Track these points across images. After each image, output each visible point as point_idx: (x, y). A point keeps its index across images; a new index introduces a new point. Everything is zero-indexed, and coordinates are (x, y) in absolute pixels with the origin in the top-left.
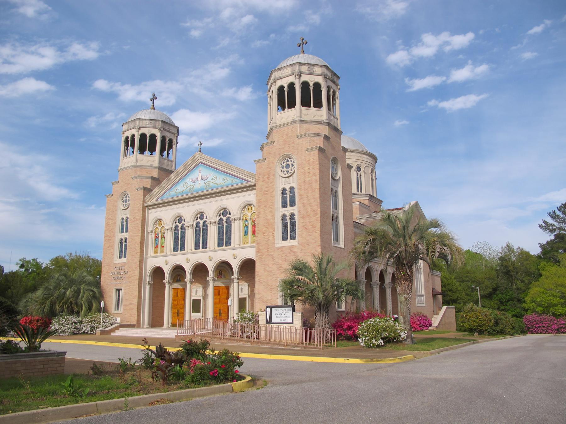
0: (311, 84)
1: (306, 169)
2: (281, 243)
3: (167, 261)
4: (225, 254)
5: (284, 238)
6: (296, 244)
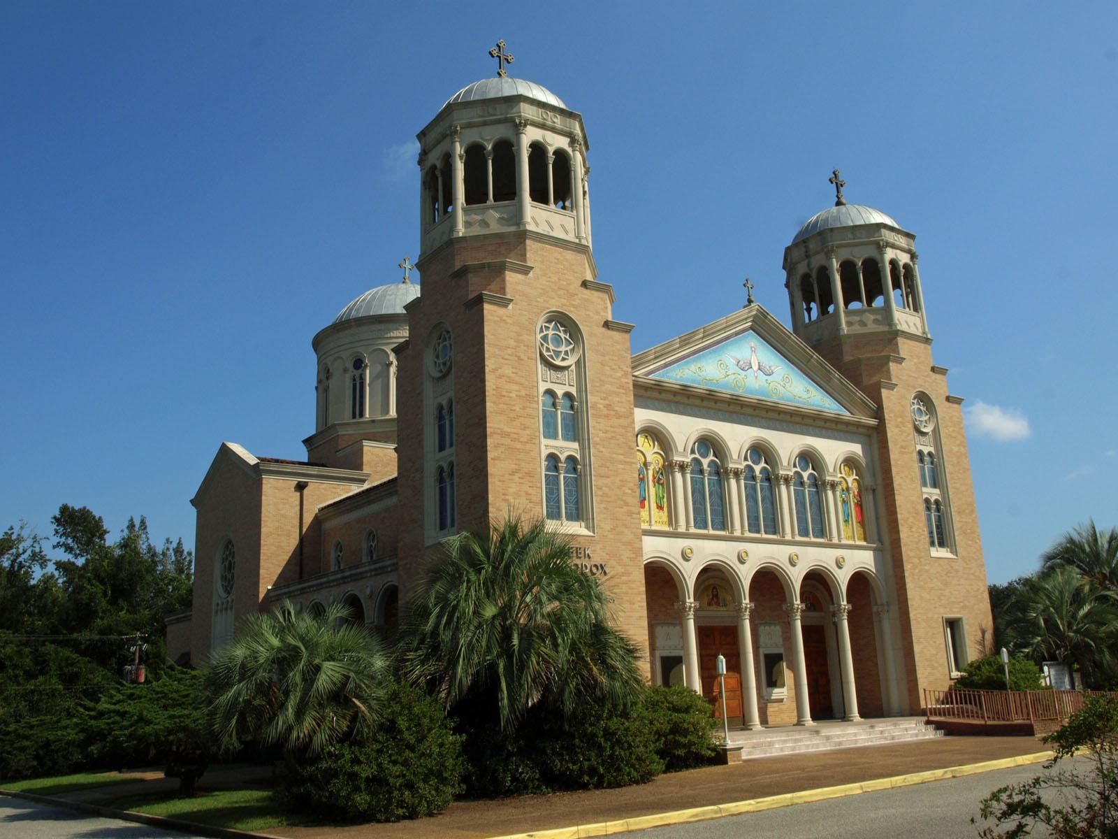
0: (551, 150)
1: (951, 429)
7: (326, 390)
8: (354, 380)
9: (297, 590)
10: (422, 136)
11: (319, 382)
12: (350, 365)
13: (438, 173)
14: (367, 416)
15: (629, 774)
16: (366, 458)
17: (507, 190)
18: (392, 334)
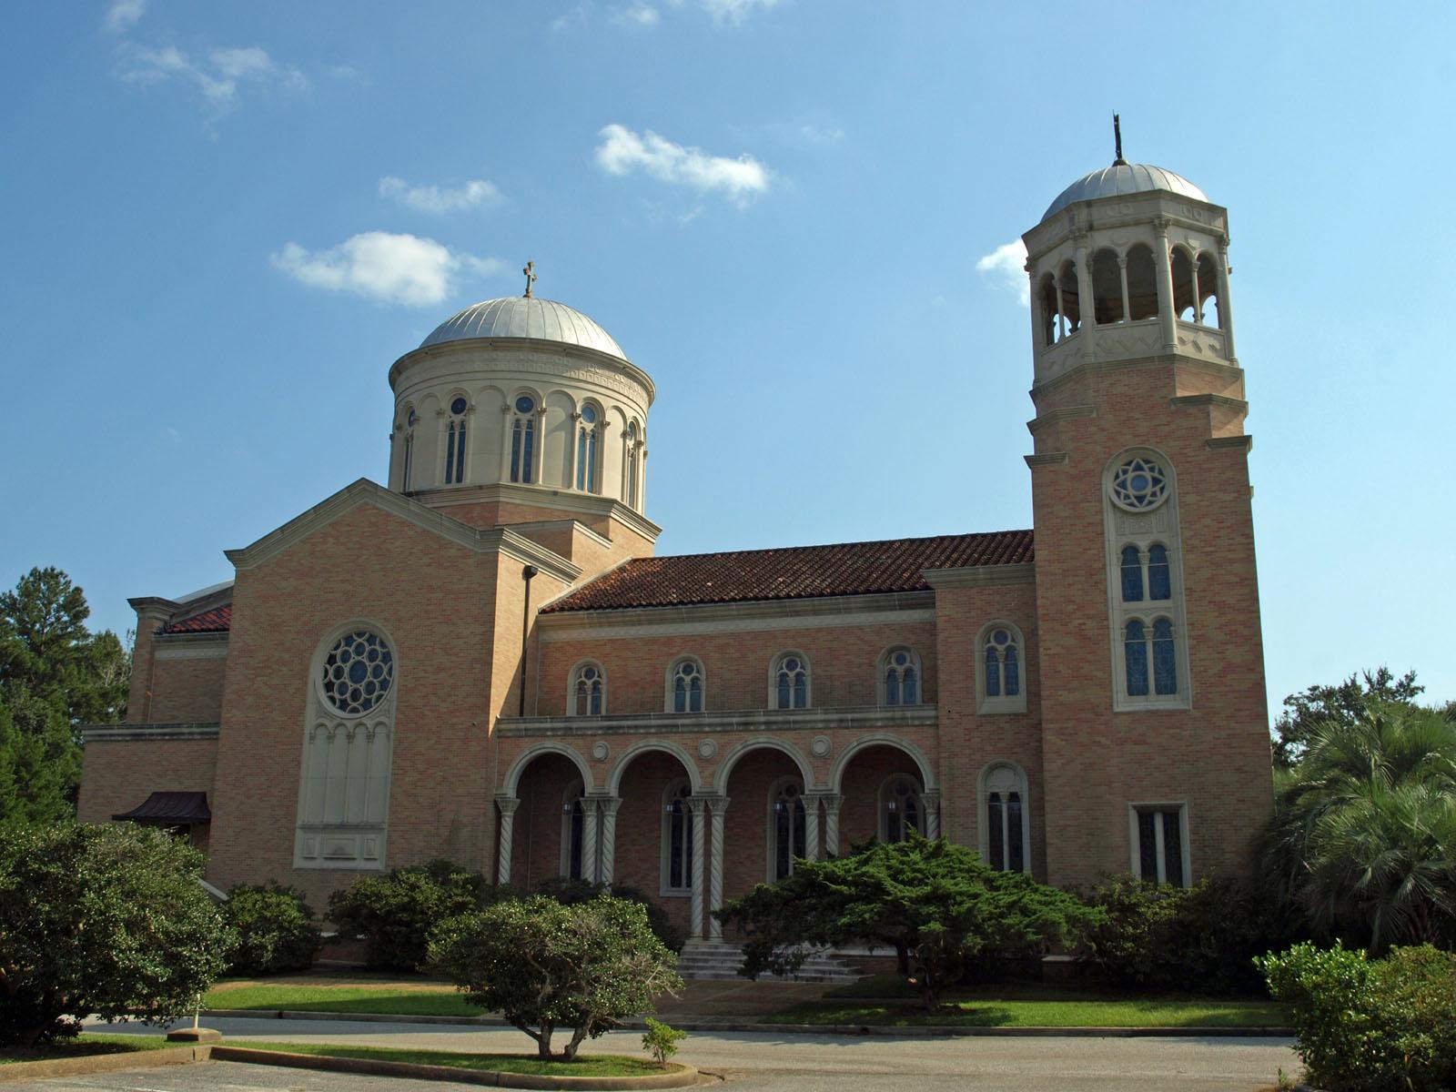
0: (1122, 254)
5: (1136, 689)
6: (1188, 706)
7: (409, 440)
8: (452, 428)
9: (600, 728)
10: (1026, 237)
11: (397, 427)
12: (446, 405)
13: (1057, 283)
14: (540, 482)
15: (170, 1005)
16: (575, 547)
17: (1147, 305)
18: (573, 375)
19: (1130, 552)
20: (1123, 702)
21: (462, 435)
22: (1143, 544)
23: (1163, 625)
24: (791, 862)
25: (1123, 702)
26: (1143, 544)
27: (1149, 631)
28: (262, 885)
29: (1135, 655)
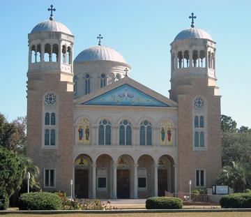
2: (195, 148)
3: (95, 151)
4: (125, 150)
5: (47, 143)
6: (43, 148)
19: (197, 117)
20: (43, 146)
21: (89, 83)
22: (50, 113)
23: (53, 131)
24: (194, 131)
25: (43, 146)
26: (50, 113)
27: (199, 118)
28: (209, 75)
29: (47, 135)
